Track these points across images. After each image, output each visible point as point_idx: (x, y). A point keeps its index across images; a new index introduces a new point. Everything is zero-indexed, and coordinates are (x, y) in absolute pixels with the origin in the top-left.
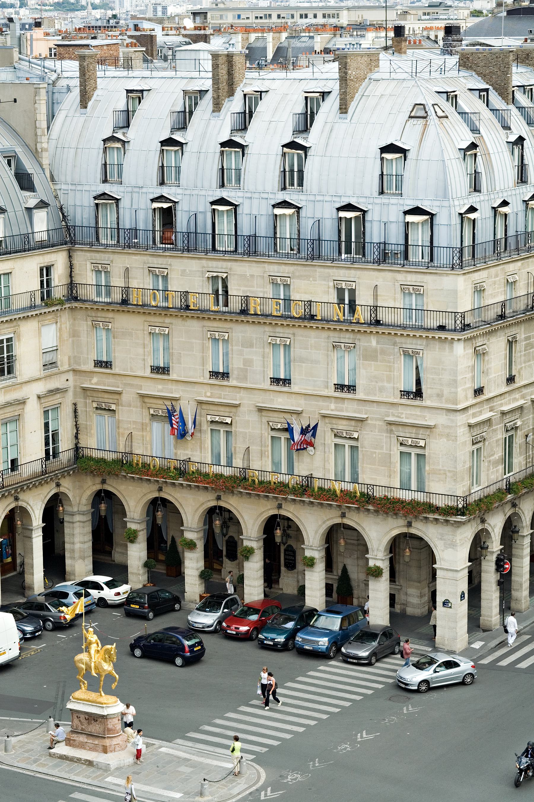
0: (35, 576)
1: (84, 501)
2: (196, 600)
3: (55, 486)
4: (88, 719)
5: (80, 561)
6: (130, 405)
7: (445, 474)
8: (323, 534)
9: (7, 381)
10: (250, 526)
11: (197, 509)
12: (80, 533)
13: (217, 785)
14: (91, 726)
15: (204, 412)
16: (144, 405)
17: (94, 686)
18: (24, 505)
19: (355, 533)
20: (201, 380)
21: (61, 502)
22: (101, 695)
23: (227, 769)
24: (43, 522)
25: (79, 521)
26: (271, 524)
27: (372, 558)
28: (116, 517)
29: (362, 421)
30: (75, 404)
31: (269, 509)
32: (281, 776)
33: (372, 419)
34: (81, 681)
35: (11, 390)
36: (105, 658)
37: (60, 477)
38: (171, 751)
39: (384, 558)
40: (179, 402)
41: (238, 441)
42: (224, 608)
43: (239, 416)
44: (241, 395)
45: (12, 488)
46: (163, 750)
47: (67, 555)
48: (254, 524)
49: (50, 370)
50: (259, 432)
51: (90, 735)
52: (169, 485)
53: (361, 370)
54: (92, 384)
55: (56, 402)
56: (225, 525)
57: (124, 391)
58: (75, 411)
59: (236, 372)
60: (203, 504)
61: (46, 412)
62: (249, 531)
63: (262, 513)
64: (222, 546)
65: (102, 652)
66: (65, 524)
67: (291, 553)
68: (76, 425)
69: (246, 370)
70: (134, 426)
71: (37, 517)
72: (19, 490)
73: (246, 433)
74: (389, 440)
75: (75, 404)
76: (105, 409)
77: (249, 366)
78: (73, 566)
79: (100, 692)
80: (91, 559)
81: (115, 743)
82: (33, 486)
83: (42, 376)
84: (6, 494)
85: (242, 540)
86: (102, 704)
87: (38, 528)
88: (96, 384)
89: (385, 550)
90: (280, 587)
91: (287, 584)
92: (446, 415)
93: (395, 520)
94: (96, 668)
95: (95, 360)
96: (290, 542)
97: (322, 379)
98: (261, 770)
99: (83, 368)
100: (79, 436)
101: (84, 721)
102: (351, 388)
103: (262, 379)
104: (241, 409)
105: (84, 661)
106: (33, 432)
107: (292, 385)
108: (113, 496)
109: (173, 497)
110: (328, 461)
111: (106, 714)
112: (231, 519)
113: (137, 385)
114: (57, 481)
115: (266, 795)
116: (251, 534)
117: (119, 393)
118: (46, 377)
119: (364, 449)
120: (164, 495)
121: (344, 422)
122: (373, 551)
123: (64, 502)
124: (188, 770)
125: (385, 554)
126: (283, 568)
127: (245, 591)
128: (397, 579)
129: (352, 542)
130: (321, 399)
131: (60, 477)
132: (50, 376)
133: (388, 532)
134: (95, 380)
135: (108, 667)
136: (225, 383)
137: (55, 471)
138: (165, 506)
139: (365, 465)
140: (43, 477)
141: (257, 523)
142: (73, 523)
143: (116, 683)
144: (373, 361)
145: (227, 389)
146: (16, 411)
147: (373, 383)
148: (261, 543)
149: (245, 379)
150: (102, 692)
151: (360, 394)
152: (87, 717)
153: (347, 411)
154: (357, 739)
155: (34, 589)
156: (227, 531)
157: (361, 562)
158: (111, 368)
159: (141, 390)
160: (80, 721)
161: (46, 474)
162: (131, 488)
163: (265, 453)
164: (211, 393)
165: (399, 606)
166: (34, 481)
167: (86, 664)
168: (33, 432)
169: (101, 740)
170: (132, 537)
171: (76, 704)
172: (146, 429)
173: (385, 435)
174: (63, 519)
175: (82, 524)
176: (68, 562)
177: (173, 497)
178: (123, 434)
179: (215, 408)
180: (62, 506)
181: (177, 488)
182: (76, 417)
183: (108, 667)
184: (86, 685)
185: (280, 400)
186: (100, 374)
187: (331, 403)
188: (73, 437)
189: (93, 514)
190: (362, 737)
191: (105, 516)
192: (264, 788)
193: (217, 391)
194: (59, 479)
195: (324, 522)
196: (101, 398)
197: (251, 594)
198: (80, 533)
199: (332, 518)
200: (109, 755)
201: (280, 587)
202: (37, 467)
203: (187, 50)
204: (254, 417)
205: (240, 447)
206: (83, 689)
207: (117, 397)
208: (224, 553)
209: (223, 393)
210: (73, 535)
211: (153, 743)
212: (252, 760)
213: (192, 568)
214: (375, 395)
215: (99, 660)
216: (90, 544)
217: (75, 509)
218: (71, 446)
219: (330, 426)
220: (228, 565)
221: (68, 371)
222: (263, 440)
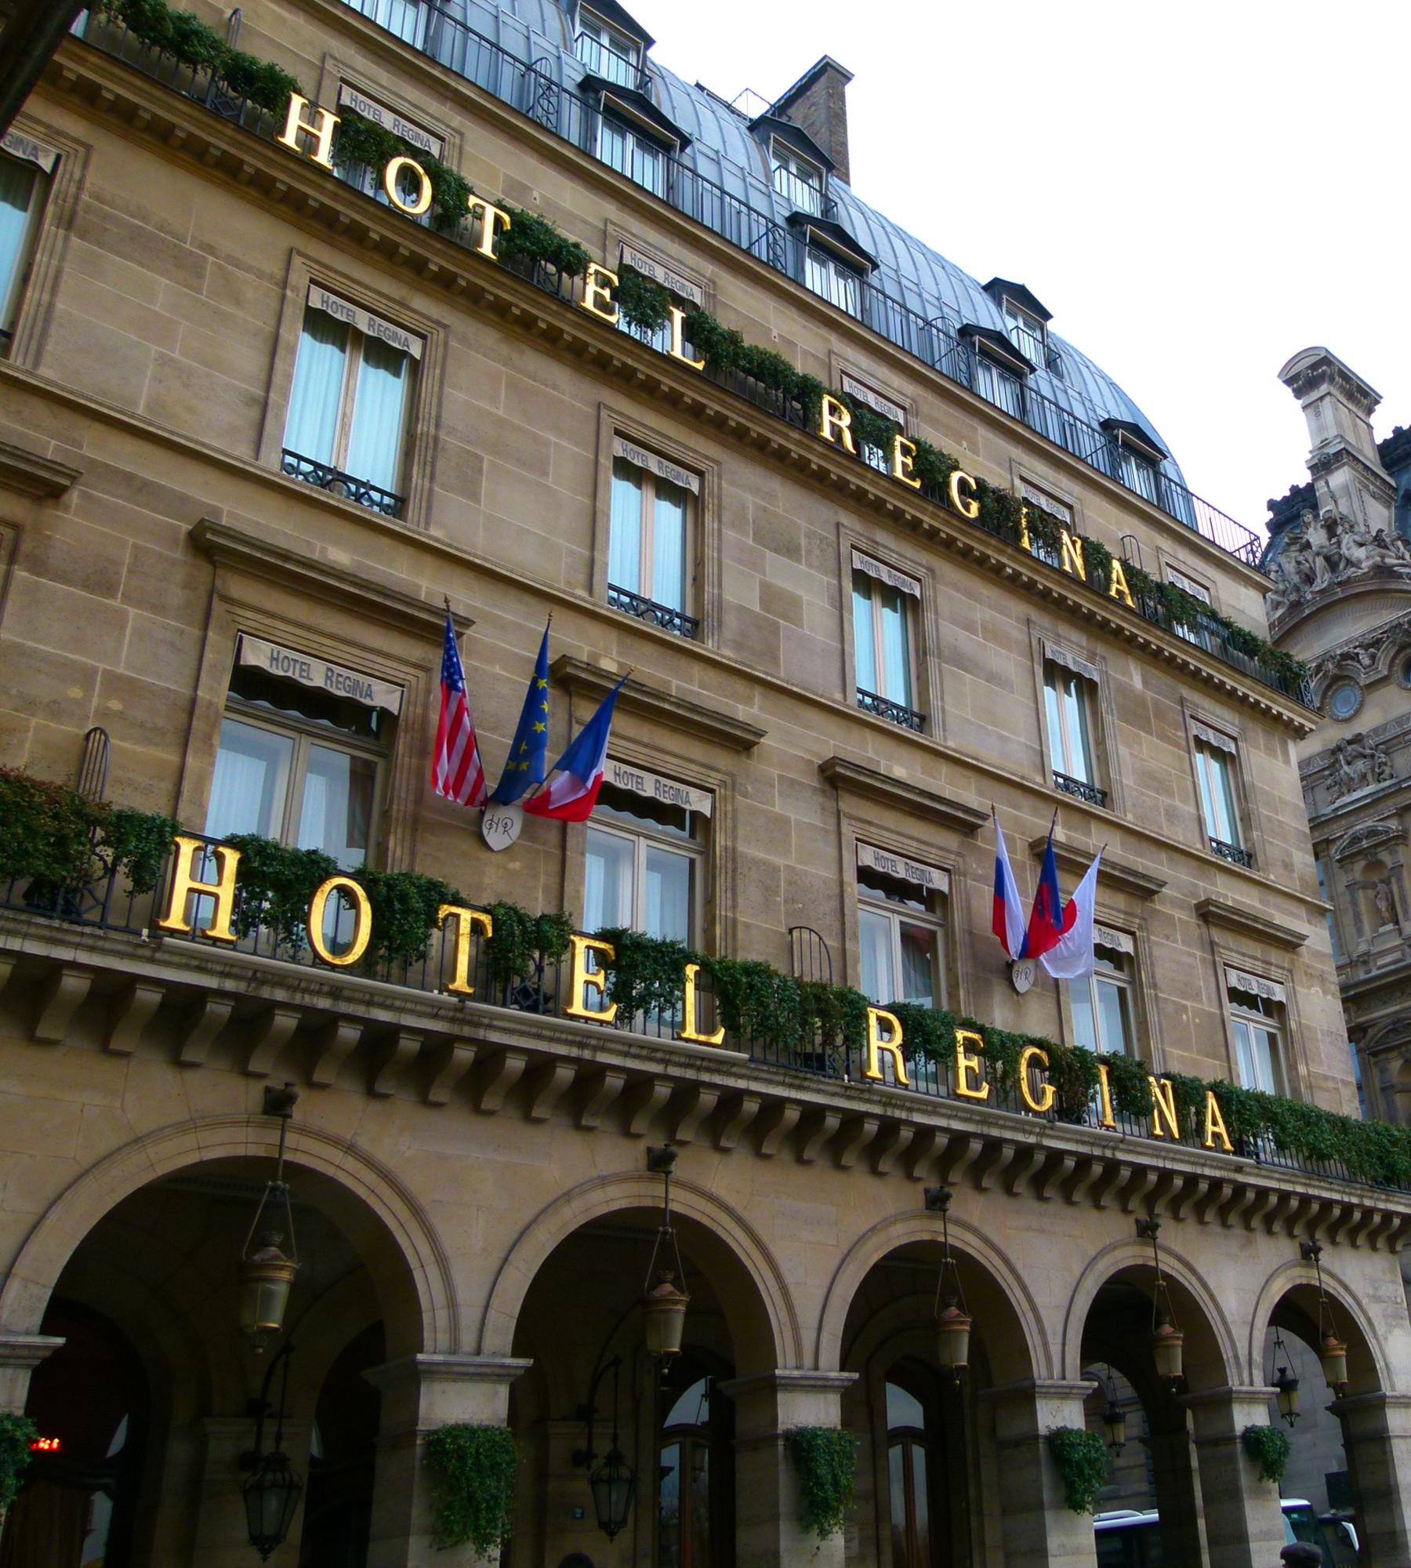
7: (1337, 1089)
41: (740, 901)
42: (193, 46)
44: (755, 710)
60: (567, 1196)
69: (775, 629)
77: (786, 618)
92: (1310, 922)
97: (1022, 739)
203: (543, 21)
204: (804, 812)
205: (748, 926)
207: (724, 760)
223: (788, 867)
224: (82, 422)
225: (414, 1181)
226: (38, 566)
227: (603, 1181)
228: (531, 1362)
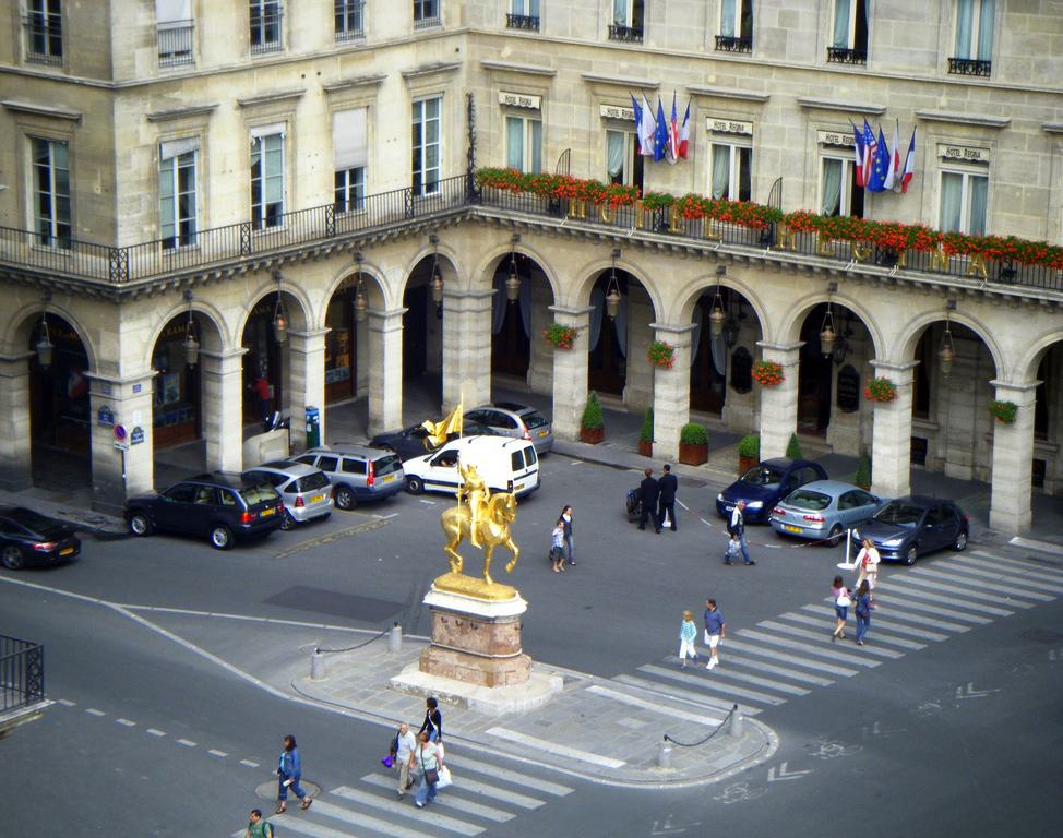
0: (386, 401)
1: (479, 273)
2: (672, 457)
3: (428, 241)
4: (462, 624)
5: (469, 382)
6: (567, 99)
8: (911, 341)
9: (348, 42)
10: (775, 324)
11: (681, 292)
12: (471, 332)
13: (690, 751)
14: (466, 637)
15: (701, 113)
16: (594, 98)
17: (474, 568)
18: (371, 271)
19: (974, 346)
20: (700, 52)
21: (438, 273)
22: (486, 582)
23: (707, 727)
24: (405, 305)
25: (469, 310)
26: (814, 320)
27: (1003, 387)
28: (536, 310)
29: (998, 128)
30: (470, 97)
31: (813, 294)
32: (807, 746)
33: (1018, 125)
34: (451, 556)
35: (354, 60)
36: (496, 515)
37: (437, 225)
38: (608, 692)
39: (1025, 387)
40: (658, 92)
43: (765, 121)
45: (352, 238)
46: (595, 688)
47: (446, 369)
48: (783, 322)
49: (426, 29)
50: (801, 149)
51: (464, 653)
52: (632, 247)
53: (1004, 31)
54: (502, 59)
55: (436, 88)
56: (730, 326)
57: (558, 74)
58: (470, 109)
59: (764, 38)
60: (693, 282)
61: (416, 106)
62: (774, 333)
63: (799, 301)
64: (723, 366)
65: (491, 505)
66: (445, 314)
67: (851, 381)
68: (470, 135)
70: (575, 138)
71: (394, 294)
72: (363, 243)
73: (777, 151)
74: (1048, 164)
75: (470, 97)
76: (519, 108)
77: (791, 25)
78: (455, 390)
79: (484, 577)
80: (488, 379)
81: (509, 670)
82: (387, 239)
83: (412, 37)
84: (340, 248)
85: (760, 349)
86: (488, 597)
87: (394, 316)
88: (509, 58)
89: (1030, 370)
90: (829, 441)
91: (840, 434)
93: (1051, 316)
94: (480, 534)
95: (508, 15)
96: (852, 360)
97: (927, 50)
98: (772, 734)
99: (487, 28)
100: (475, 154)
101: (455, 627)
102: (981, 66)
103: (813, 50)
104: (770, 106)
105: (459, 520)
106: (392, 142)
107: (869, 61)
108: (533, 272)
109: (639, 269)
110: (927, 203)
111: (493, 616)
112: (742, 316)
113: (583, 61)
114: (433, 233)
115: (777, 774)
116: (778, 339)
117: (549, 76)
118: (419, 41)
119: (998, 182)
120: (622, 265)
121: (964, 132)
122: (1005, 373)
123: (444, 274)
124: (636, 724)
125: (1028, 380)
126: (834, 409)
127: (762, 443)
128: (1049, 434)
129: (968, 362)
130: (921, 88)
131: (437, 225)
132: (426, 39)
133: (1037, 340)
134: (507, 51)
135: (497, 531)
136: (744, 58)
137: (428, 214)
138: (624, 290)
139: (998, 213)
140: (407, 222)
141: (789, 318)
142: (459, 312)
143: (514, 562)
144: (1029, 11)
145: (748, 69)
146: (361, 98)
147: (1026, 56)
148: (795, 356)
149: (782, 49)
150: (488, 578)
151: (999, 78)
152: (460, 621)
153: (970, 108)
154: (955, 694)
155: (383, 424)
156: (735, 337)
157: (982, 400)
158: (537, 30)
159: (590, 70)
160: (447, 627)
161: (413, 217)
162: (563, 251)
163: (810, 191)
164: (717, 77)
165: (1051, 484)
166: (391, 229)
167: (463, 526)
168: (392, 142)
169: (486, 662)
170: (565, 340)
171: (440, 596)
172: (596, 143)
173: (1041, 154)
174: (441, 302)
175: (473, 315)
176: (447, 382)
177: (639, 269)
178: (553, 152)
179: (724, 105)
180: (440, 279)
181: (647, 252)
182: (470, 118)
183: (497, 531)
184: (460, 564)
185: (844, 90)
186: (516, 41)
187: (940, 95)
188: (465, 157)
189: (495, 298)
190: (965, 692)
191: (517, 301)
192: (775, 762)
193: (729, 73)
194: (436, 230)
195: (914, 320)
196: (517, 85)
197: (772, 448)
198: (471, 332)
199: (930, 312)
200: (497, 689)
201: (829, 441)
202: (397, 204)
204: (794, 123)
205: (764, 178)
206: (455, 571)
207: (543, 83)
208: (729, 379)
209: (738, 77)
210: (458, 334)
211: (577, 676)
212: (756, 717)
213: (668, 399)
214: (1028, 78)
215: (485, 519)
216: (488, 352)
217: (464, 288)
218: (461, 170)
219: (935, 139)
220: (734, 404)
221: (458, 34)
222: (808, 165)
223: (784, 151)
224: (911, 75)
225: (651, 274)
226: (554, 99)
227: (703, 277)
228: (758, 343)
